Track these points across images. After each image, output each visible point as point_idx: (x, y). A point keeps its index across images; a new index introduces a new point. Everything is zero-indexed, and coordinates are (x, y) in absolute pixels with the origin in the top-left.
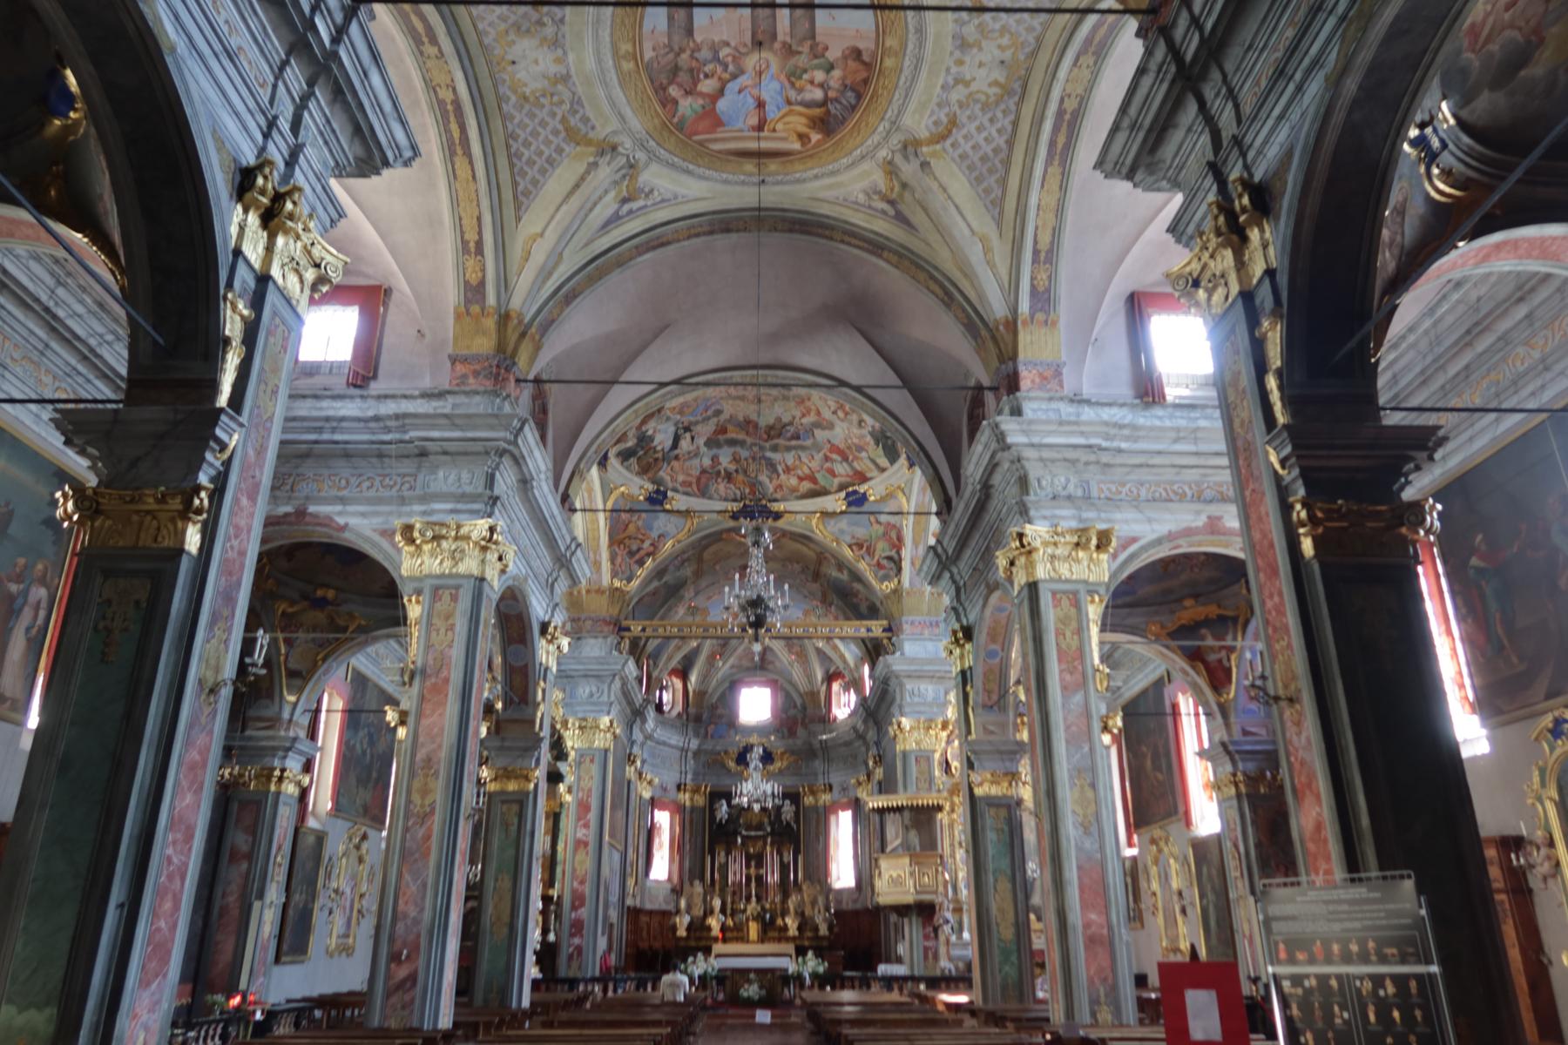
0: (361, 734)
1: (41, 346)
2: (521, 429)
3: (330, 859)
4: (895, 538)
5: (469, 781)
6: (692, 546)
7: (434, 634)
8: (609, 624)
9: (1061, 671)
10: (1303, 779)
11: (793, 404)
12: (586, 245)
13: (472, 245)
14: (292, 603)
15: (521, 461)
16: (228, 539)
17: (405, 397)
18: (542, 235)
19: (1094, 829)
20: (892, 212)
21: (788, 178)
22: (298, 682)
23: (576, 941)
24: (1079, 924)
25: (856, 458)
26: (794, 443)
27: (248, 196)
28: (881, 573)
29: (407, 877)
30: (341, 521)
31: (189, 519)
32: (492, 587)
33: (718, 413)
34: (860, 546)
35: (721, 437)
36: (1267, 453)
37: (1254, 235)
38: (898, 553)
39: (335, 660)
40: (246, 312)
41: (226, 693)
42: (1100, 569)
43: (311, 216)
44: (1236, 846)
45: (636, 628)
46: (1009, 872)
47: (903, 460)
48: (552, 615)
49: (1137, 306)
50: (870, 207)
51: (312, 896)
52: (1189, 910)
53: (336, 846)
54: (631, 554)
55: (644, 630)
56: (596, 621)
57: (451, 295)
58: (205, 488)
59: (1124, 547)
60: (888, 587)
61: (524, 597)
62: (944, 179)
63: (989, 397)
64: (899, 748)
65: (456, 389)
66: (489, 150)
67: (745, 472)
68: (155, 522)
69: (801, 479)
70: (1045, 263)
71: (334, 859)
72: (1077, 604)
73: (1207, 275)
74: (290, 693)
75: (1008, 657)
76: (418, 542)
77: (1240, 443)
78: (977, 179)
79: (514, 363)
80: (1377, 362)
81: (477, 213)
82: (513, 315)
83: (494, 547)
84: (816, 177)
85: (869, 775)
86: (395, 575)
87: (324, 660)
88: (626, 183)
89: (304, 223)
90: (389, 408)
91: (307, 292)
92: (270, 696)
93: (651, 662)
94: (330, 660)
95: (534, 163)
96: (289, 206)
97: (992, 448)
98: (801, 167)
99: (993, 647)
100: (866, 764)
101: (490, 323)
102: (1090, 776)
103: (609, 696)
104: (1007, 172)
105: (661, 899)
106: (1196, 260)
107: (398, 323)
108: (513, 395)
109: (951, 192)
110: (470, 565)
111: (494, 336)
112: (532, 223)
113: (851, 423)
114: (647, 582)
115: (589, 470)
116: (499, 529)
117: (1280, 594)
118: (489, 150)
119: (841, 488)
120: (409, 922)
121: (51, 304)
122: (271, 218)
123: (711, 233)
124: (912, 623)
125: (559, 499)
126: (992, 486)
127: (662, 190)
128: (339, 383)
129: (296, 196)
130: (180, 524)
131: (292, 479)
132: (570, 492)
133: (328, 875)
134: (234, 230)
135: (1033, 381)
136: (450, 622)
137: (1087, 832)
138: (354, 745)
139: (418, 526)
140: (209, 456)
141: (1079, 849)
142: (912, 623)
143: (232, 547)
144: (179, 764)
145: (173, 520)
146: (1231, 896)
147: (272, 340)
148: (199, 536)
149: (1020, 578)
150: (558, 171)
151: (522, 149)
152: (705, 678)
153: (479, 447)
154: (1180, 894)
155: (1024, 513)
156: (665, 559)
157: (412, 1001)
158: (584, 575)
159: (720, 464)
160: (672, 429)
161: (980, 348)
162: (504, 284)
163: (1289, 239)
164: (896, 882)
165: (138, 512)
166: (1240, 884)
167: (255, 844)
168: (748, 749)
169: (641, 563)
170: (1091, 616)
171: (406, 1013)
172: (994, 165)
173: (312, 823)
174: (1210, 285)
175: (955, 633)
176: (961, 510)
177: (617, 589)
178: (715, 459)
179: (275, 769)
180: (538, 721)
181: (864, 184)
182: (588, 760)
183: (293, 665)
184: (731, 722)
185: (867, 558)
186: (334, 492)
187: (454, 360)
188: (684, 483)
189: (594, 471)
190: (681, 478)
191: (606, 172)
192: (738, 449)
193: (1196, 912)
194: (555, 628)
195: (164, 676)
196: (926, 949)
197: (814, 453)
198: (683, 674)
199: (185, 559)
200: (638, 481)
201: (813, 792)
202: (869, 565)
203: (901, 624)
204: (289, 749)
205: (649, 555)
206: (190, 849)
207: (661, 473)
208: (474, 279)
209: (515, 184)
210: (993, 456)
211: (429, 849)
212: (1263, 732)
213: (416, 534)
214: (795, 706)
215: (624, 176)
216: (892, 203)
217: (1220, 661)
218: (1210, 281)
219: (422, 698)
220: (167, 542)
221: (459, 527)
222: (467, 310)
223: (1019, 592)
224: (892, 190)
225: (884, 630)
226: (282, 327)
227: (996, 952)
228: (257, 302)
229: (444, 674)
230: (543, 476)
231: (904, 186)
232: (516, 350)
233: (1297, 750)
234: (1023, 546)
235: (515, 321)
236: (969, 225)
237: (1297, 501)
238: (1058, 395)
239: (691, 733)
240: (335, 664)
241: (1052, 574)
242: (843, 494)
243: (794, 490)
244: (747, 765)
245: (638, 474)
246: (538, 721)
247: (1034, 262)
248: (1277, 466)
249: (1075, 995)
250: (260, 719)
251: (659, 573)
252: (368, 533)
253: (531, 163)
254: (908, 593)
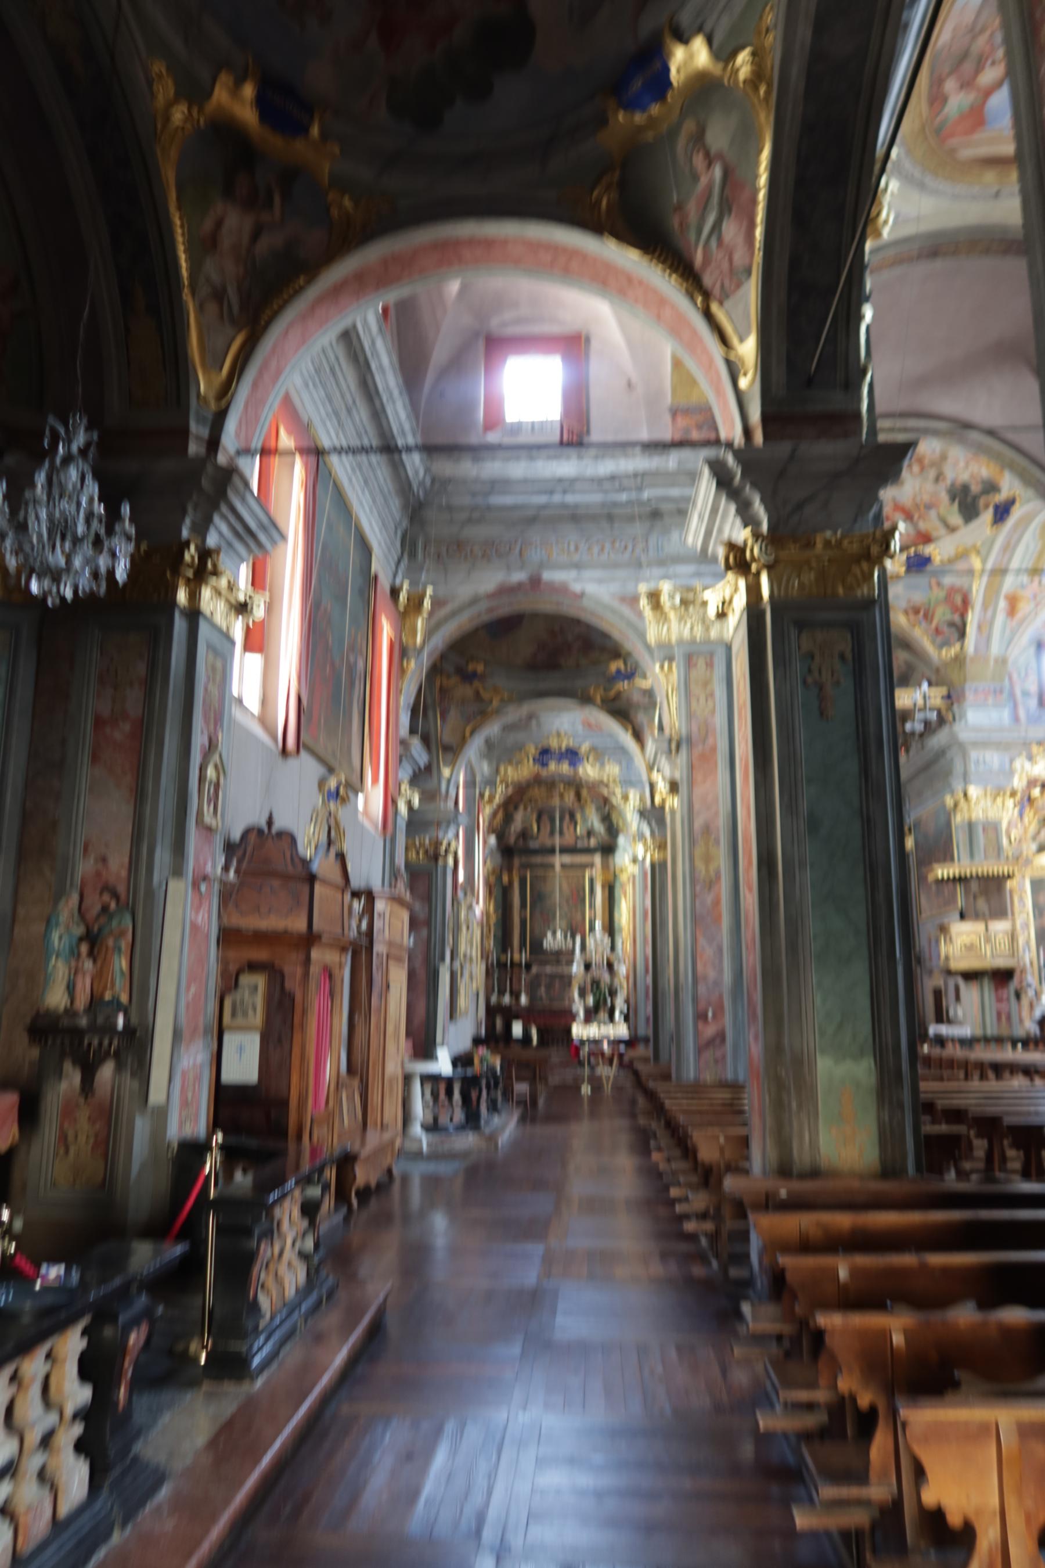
7: (694, 704)
22: (450, 756)
28: (939, 639)
29: (702, 941)
34: (916, 611)
64: (958, 819)
107: (597, 370)
157: (724, 1057)
185: (924, 624)
187: (675, 412)
196: (999, 1015)
219: (691, 767)
229: (710, 741)
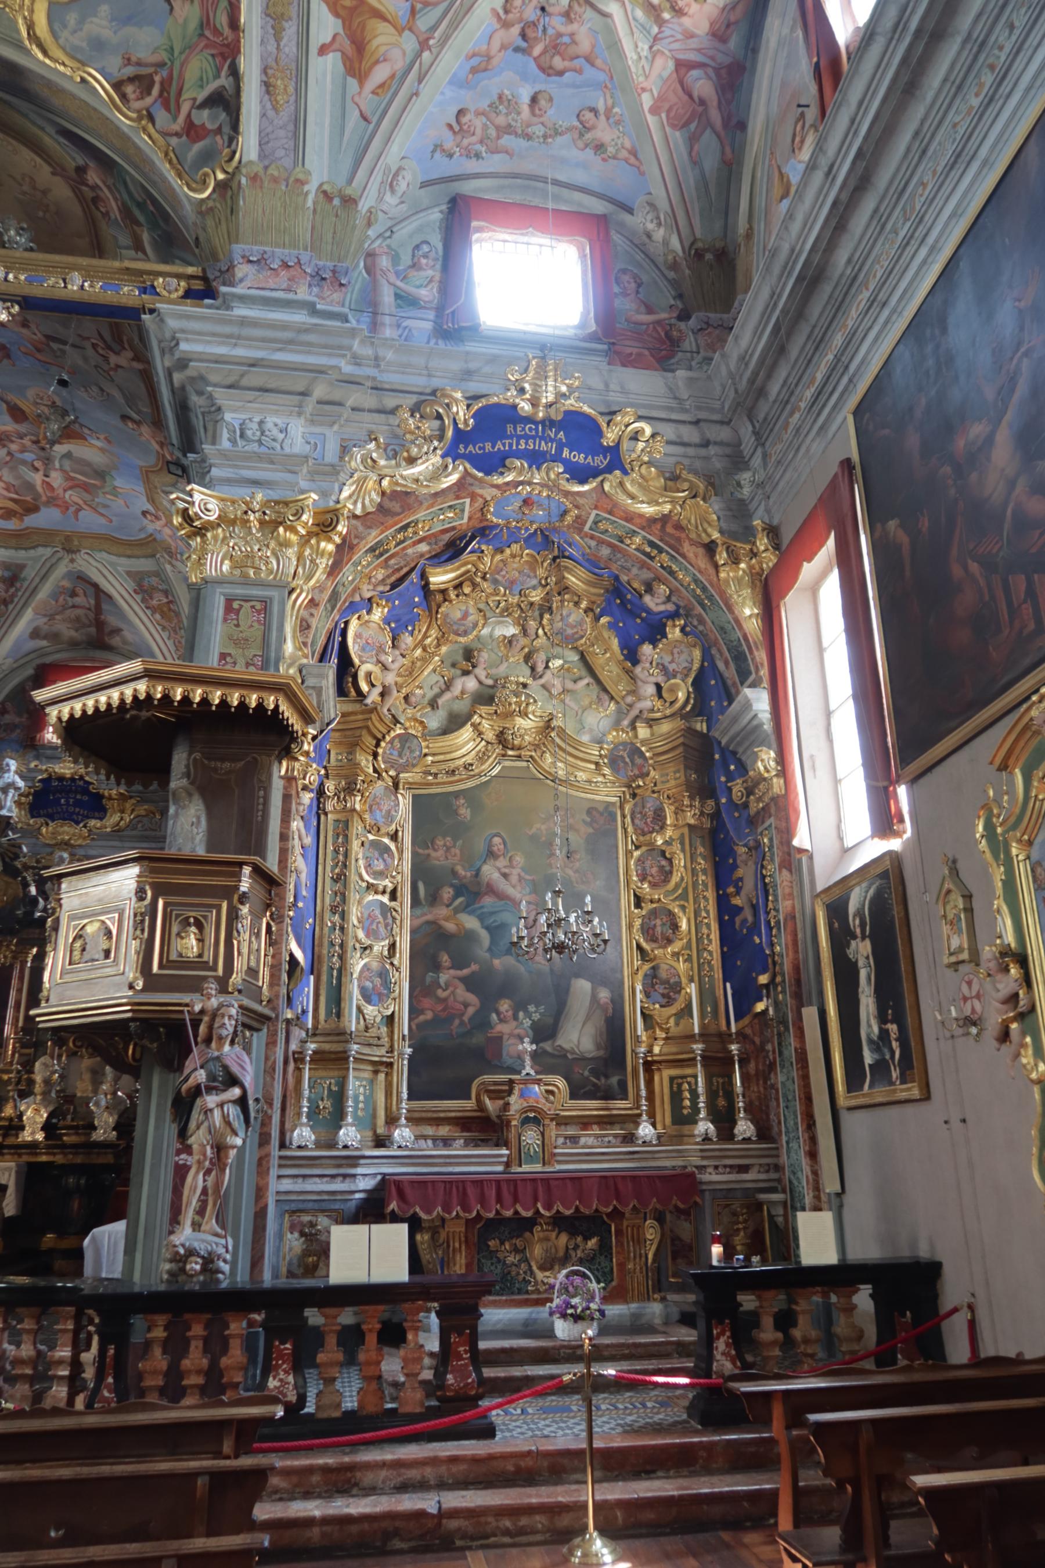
142: (261, 262)
254: (254, 178)
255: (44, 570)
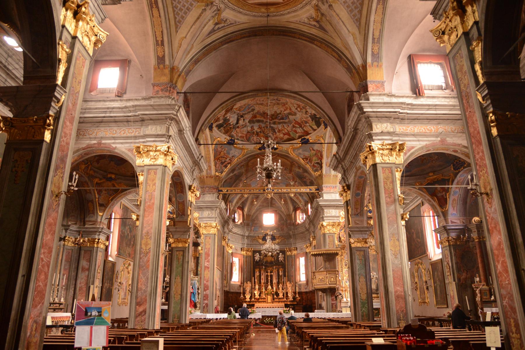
0: (127, 228)
1: (4, 80)
2: (179, 110)
3: (117, 272)
4: (319, 155)
5: (163, 241)
6: (245, 160)
7: (148, 186)
8: (214, 189)
9: (386, 197)
10: (493, 225)
11: (281, 106)
12: (202, 41)
13: (160, 42)
14: (100, 179)
15: (179, 122)
16: (61, 137)
17: (136, 100)
18: (185, 37)
19: (399, 256)
20: (318, 26)
21: (278, 14)
22: (103, 208)
23: (206, 302)
24: (393, 291)
25: (305, 126)
26: (281, 121)
27: (67, 4)
30: (114, 146)
31: (46, 128)
32: (169, 170)
33: (253, 110)
35: (254, 119)
36: (476, 95)
37: (469, 9)
38: (321, 161)
39: (115, 200)
40: (67, 50)
41: (63, 197)
42: (400, 159)
43: (93, 15)
44: (448, 264)
45: (225, 191)
46: (364, 275)
47: (322, 126)
48: (193, 183)
49: (411, 61)
50: (309, 24)
51: (112, 284)
52: (429, 288)
53: (119, 267)
54: (222, 163)
55: (227, 191)
56: (210, 188)
57: (153, 61)
58: (51, 116)
59: (409, 150)
60: (317, 173)
61: (182, 175)
62: (338, 11)
63: (356, 95)
65: (155, 96)
66: (165, 5)
67: (264, 132)
68: (33, 130)
69: (284, 134)
70: (377, 43)
71: (119, 272)
72: (392, 172)
73: (449, 28)
74: (100, 212)
75: (364, 195)
76: (142, 152)
77: (464, 94)
78: (350, 11)
79: (176, 86)
80: (520, 58)
81: (161, 30)
82: (175, 68)
83: (169, 154)
84: (289, 13)
85: (311, 244)
86: (134, 165)
87: (112, 200)
88: (217, 17)
89: (90, 17)
90: (130, 104)
91: (92, 45)
92: (94, 213)
93: (230, 204)
94: (114, 200)
95: (182, 10)
96: (83, 9)
97: (358, 114)
98: (283, 9)
99: (358, 192)
100: (310, 240)
101: (167, 71)
102: (396, 236)
103: (215, 215)
104: (362, 8)
105: (236, 288)
106: (444, 23)
108: (176, 98)
109: (340, 16)
110: (161, 161)
111: (169, 76)
112: (183, 31)
113: (303, 113)
114: (228, 174)
115: (205, 130)
116: (171, 147)
117: (483, 152)
118: (165, 5)
119: (300, 137)
120: (143, 291)
121: (6, 64)
122: (76, 15)
123: (249, 36)
124: (327, 187)
125: (194, 140)
126: (358, 129)
127: (230, 20)
128: (113, 96)
129: (86, 5)
130: (42, 130)
131: (96, 131)
132: (199, 138)
133: (117, 278)
134: (62, 17)
135: (373, 88)
136: (154, 182)
137: (396, 258)
138: (124, 232)
139: (141, 147)
140: (53, 104)
141: (393, 264)
142: (327, 187)
143: (63, 141)
144: (45, 223)
145: (40, 129)
146: (446, 282)
147: (78, 62)
148: (50, 135)
149: (370, 162)
150: (191, 13)
151: (178, 5)
152: (249, 210)
153: (163, 117)
154: (426, 282)
155: (370, 137)
156: (235, 165)
158: (205, 168)
159: (254, 129)
160: (236, 116)
161: (352, 77)
162: (172, 56)
163: (485, 8)
164: (321, 280)
165: (27, 126)
166: (449, 278)
167: (90, 266)
168: (266, 235)
169: (226, 166)
170: (397, 176)
171: (143, 324)
172: (357, 5)
173: (110, 259)
174: (450, 32)
175: (343, 187)
176: (346, 140)
177: (217, 176)
178: (252, 127)
179: (96, 239)
180: (189, 221)
181: (307, 15)
182: (208, 238)
183: (101, 202)
184: (261, 226)
185: (309, 163)
186: (111, 135)
187: (154, 85)
188: (241, 137)
189: (207, 130)
190: (240, 135)
191: (209, 13)
192: (261, 124)
193: (432, 289)
194: (194, 187)
195: (37, 189)
196: (333, 304)
197: (289, 125)
198: (242, 208)
199: (44, 144)
200: (224, 136)
201: (290, 251)
202: (310, 166)
203: (322, 187)
204: (100, 232)
205: (229, 163)
206: (51, 256)
207: (233, 133)
208: (160, 55)
209: (175, 18)
210: (358, 117)
211: (149, 265)
212: (459, 222)
213: (141, 149)
214: (283, 220)
215: (216, 14)
216: (318, 22)
217: (443, 196)
218: (450, 30)
220: (38, 138)
221: (156, 147)
222: (158, 67)
223: (369, 168)
224: (318, 16)
225: (316, 190)
226: (82, 58)
227: (360, 303)
228: (72, 47)
230: (188, 129)
231: (323, 15)
232: (176, 81)
233: (490, 214)
234: (371, 150)
235: (176, 70)
236: (347, 29)
237: (490, 113)
238: (383, 93)
239: (246, 230)
240: (115, 202)
241: (382, 161)
242: (300, 140)
243: (282, 139)
244: (266, 241)
245: (224, 133)
246: (189, 221)
247: (373, 43)
248: (481, 100)
249: (392, 317)
250: (90, 221)
251: (233, 170)
252: (124, 150)
253: (181, 10)
254: (325, 176)
255: (171, 54)
